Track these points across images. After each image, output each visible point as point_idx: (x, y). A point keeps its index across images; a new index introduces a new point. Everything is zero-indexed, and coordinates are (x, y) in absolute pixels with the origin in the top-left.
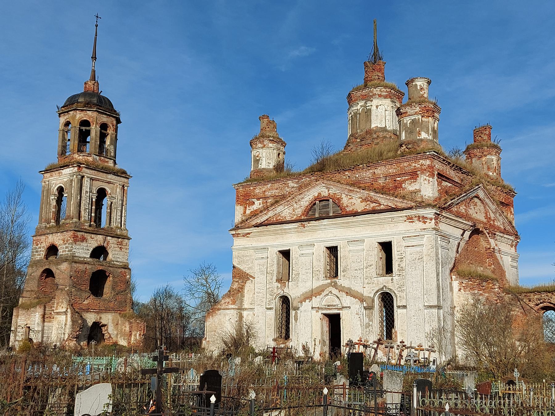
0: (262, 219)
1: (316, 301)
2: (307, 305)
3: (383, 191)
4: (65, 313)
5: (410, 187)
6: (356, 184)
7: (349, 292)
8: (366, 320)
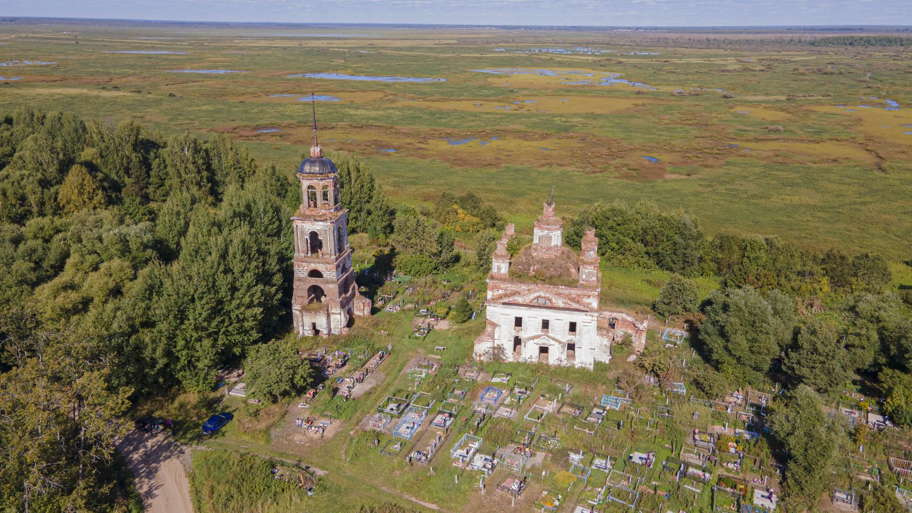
0: (506, 300)
1: (536, 341)
2: (531, 342)
3: (573, 300)
4: (340, 314)
5: (586, 300)
6: (560, 295)
7: (554, 339)
8: (561, 351)
